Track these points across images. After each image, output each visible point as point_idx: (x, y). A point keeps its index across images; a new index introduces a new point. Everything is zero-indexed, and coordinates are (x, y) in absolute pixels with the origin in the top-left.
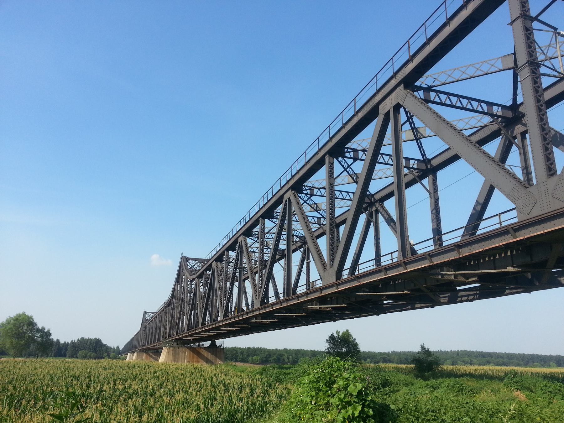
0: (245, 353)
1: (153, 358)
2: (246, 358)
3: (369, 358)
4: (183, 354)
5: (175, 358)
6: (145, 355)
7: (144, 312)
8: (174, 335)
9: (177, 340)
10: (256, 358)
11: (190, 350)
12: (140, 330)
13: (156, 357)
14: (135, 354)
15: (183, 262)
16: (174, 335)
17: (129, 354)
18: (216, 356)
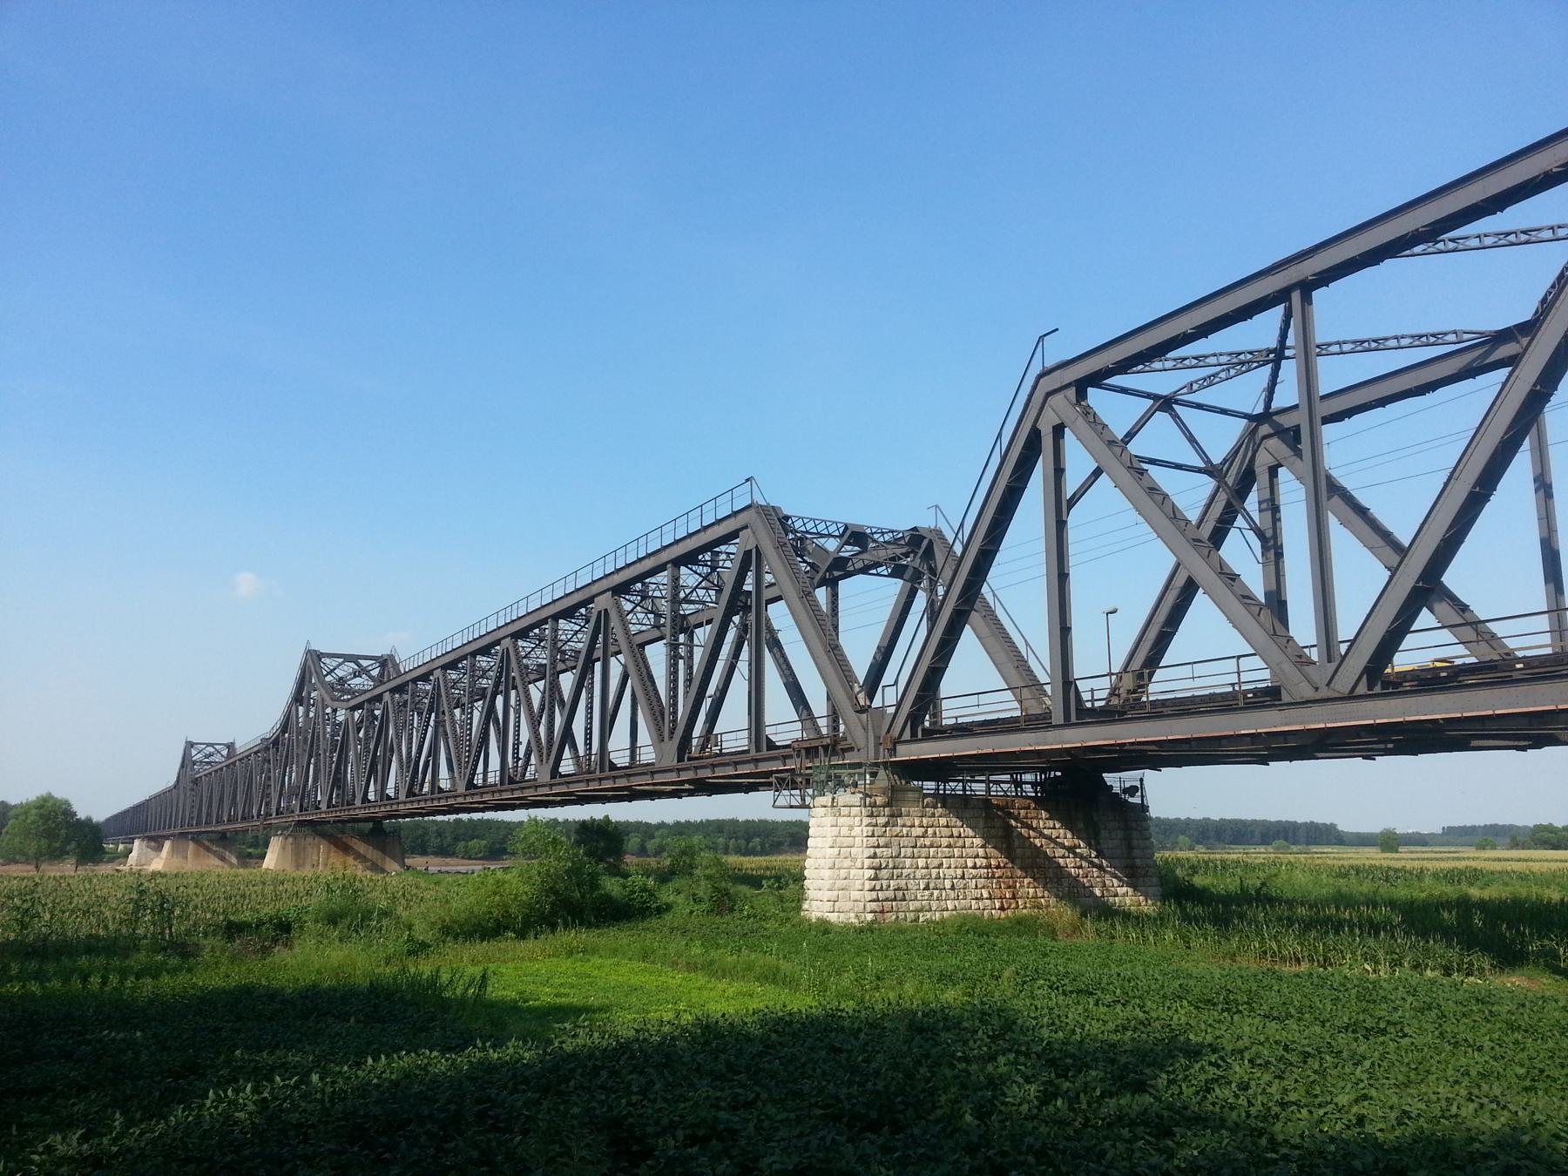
0: (448, 834)
1: (215, 853)
2: (449, 845)
3: (759, 836)
4: (315, 850)
5: (299, 859)
6: (191, 845)
7: (187, 742)
8: (293, 812)
9: (300, 823)
10: (477, 845)
11: (330, 843)
12: (176, 786)
13: (221, 850)
14: (167, 845)
15: (310, 662)
16: (293, 812)
17: (137, 842)
18: (384, 851)
